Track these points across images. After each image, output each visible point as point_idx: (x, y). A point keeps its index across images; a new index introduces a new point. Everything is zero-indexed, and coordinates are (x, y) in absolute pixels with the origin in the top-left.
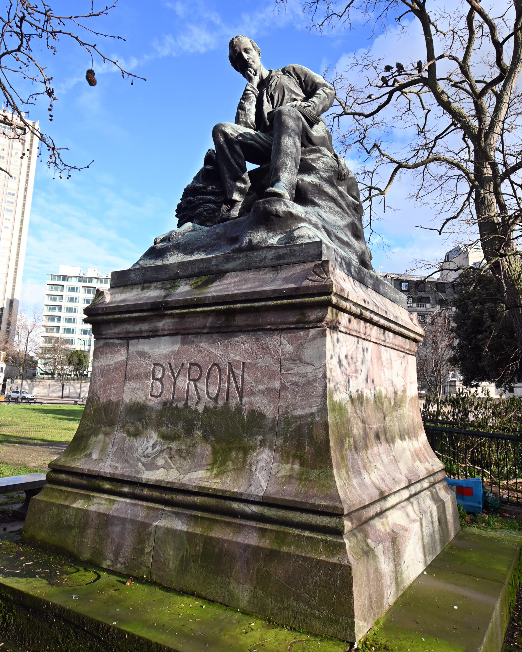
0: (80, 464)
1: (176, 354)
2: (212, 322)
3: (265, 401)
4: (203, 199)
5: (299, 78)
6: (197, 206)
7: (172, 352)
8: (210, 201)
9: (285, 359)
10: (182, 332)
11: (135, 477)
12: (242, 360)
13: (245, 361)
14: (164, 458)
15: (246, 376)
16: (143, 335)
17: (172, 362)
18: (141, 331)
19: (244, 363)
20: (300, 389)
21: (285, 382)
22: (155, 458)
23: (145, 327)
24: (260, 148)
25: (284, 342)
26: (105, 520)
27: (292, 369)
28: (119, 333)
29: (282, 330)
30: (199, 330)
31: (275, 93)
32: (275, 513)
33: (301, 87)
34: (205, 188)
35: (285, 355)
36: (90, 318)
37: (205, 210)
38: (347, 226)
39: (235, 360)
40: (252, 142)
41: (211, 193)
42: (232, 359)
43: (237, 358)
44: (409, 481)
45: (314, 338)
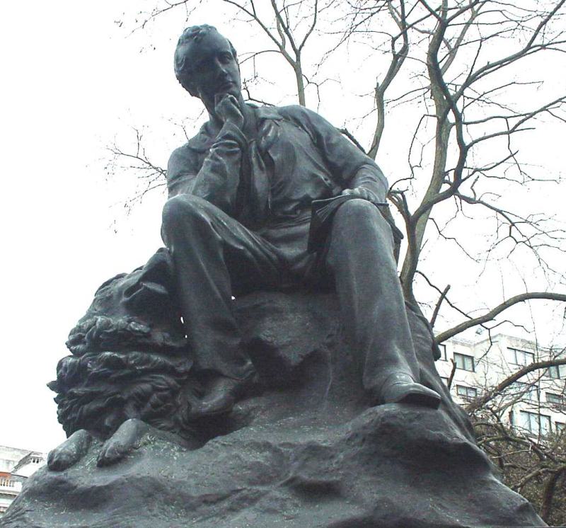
6: (134, 377)
8: (163, 369)
24: (255, 261)
34: (147, 335)
40: (242, 248)
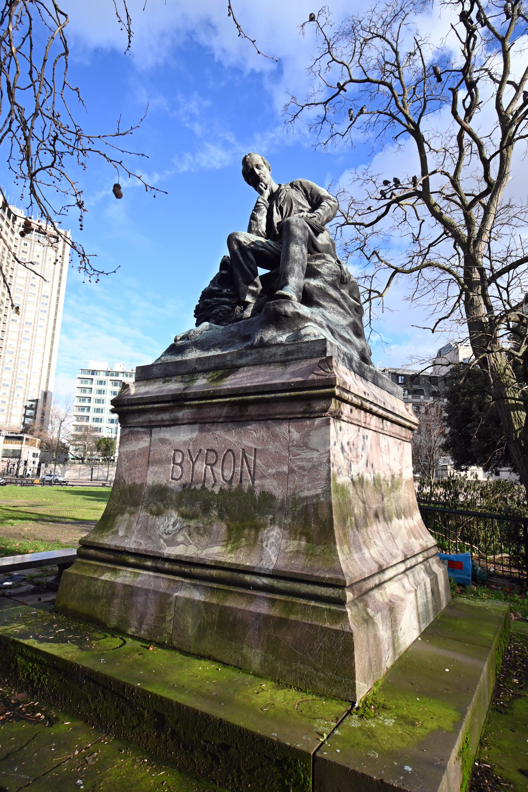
0: (107, 540)
1: (195, 441)
2: (227, 412)
3: (275, 483)
4: (218, 301)
5: (305, 191)
6: (214, 307)
7: (191, 439)
8: (225, 303)
9: (293, 446)
10: (200, 421)
11: (157, 552)
12: (254, 446)
13: (257, 447)
14: (184, 535)
15: (258, 461)
16: (164, 424)
17: (191, 448)
18: (162, 421)
19: (255, 449)
20: (306, 472)
21: (293, 466)
22: (175, 535)
23: (166, 416)
25: (292, 430)
26: (131, 591)
27: (299, 455)
28: (143, 422)
29: (290, 419)
30: (215, 420)
31: (284, 205)
32: (284, 584)
33: (308, 199)
34: (220, 291)
35: (293, 442)
36: (117, 409)
37: (220, 311)
38: (349, 325)
39: (248, 447)
41: (226, 295)
42: (245, 446)
43: (250, 445)
44: (405, 556)
45: (319, 427)
